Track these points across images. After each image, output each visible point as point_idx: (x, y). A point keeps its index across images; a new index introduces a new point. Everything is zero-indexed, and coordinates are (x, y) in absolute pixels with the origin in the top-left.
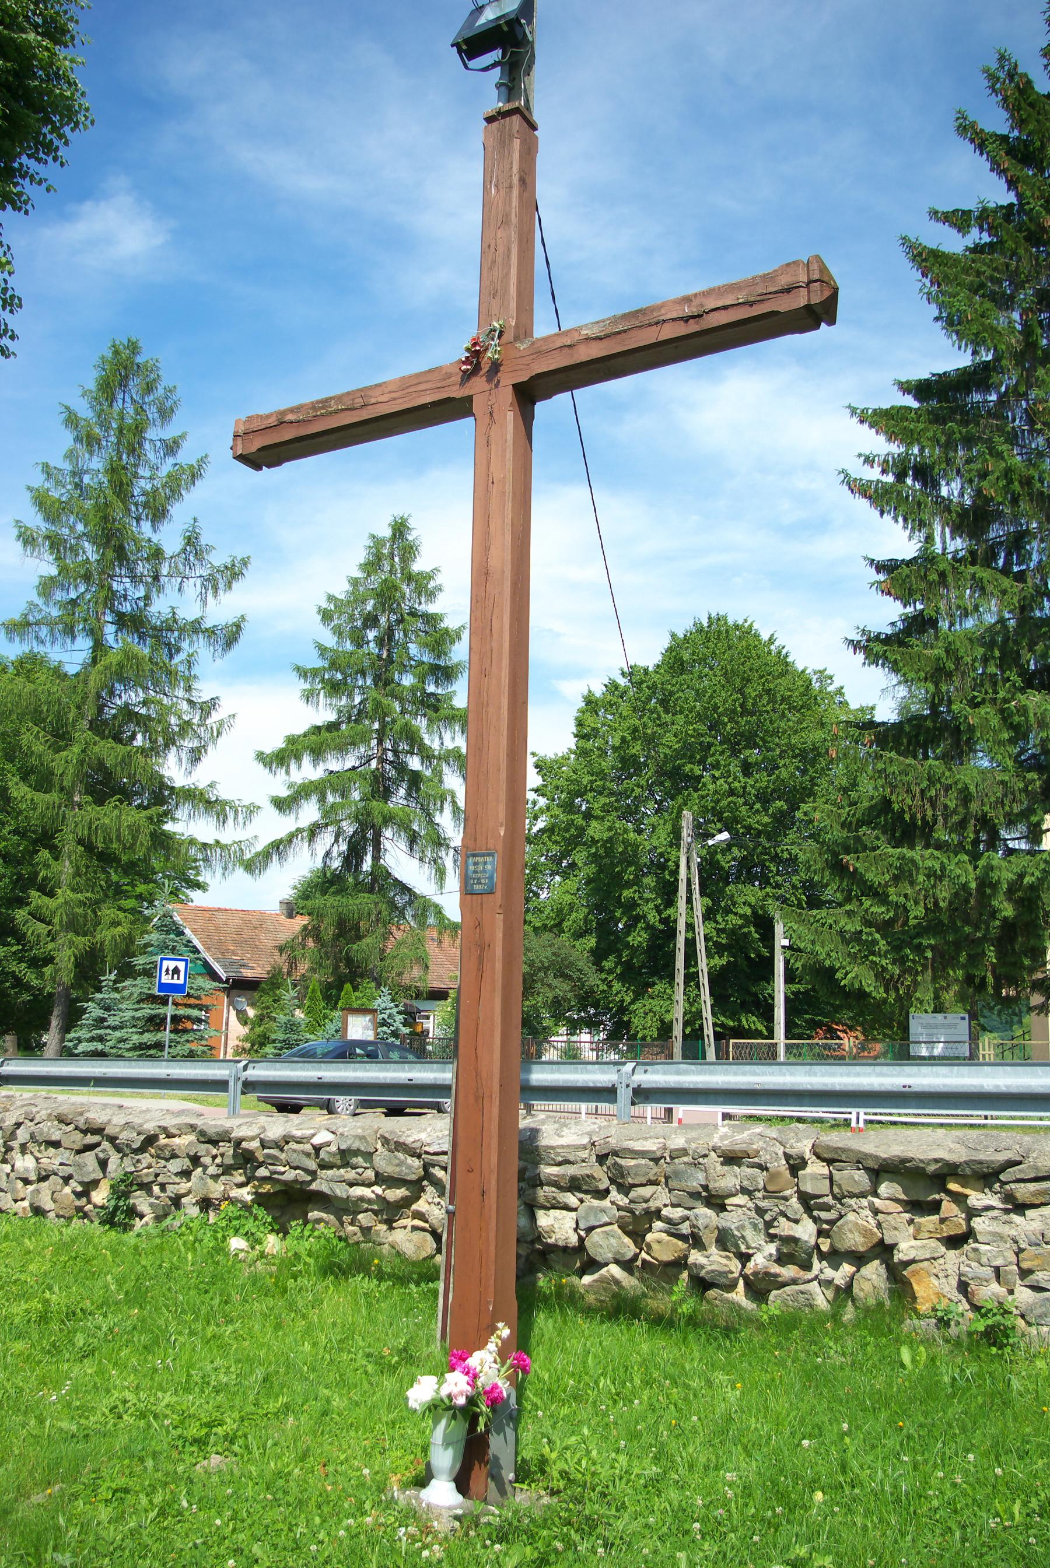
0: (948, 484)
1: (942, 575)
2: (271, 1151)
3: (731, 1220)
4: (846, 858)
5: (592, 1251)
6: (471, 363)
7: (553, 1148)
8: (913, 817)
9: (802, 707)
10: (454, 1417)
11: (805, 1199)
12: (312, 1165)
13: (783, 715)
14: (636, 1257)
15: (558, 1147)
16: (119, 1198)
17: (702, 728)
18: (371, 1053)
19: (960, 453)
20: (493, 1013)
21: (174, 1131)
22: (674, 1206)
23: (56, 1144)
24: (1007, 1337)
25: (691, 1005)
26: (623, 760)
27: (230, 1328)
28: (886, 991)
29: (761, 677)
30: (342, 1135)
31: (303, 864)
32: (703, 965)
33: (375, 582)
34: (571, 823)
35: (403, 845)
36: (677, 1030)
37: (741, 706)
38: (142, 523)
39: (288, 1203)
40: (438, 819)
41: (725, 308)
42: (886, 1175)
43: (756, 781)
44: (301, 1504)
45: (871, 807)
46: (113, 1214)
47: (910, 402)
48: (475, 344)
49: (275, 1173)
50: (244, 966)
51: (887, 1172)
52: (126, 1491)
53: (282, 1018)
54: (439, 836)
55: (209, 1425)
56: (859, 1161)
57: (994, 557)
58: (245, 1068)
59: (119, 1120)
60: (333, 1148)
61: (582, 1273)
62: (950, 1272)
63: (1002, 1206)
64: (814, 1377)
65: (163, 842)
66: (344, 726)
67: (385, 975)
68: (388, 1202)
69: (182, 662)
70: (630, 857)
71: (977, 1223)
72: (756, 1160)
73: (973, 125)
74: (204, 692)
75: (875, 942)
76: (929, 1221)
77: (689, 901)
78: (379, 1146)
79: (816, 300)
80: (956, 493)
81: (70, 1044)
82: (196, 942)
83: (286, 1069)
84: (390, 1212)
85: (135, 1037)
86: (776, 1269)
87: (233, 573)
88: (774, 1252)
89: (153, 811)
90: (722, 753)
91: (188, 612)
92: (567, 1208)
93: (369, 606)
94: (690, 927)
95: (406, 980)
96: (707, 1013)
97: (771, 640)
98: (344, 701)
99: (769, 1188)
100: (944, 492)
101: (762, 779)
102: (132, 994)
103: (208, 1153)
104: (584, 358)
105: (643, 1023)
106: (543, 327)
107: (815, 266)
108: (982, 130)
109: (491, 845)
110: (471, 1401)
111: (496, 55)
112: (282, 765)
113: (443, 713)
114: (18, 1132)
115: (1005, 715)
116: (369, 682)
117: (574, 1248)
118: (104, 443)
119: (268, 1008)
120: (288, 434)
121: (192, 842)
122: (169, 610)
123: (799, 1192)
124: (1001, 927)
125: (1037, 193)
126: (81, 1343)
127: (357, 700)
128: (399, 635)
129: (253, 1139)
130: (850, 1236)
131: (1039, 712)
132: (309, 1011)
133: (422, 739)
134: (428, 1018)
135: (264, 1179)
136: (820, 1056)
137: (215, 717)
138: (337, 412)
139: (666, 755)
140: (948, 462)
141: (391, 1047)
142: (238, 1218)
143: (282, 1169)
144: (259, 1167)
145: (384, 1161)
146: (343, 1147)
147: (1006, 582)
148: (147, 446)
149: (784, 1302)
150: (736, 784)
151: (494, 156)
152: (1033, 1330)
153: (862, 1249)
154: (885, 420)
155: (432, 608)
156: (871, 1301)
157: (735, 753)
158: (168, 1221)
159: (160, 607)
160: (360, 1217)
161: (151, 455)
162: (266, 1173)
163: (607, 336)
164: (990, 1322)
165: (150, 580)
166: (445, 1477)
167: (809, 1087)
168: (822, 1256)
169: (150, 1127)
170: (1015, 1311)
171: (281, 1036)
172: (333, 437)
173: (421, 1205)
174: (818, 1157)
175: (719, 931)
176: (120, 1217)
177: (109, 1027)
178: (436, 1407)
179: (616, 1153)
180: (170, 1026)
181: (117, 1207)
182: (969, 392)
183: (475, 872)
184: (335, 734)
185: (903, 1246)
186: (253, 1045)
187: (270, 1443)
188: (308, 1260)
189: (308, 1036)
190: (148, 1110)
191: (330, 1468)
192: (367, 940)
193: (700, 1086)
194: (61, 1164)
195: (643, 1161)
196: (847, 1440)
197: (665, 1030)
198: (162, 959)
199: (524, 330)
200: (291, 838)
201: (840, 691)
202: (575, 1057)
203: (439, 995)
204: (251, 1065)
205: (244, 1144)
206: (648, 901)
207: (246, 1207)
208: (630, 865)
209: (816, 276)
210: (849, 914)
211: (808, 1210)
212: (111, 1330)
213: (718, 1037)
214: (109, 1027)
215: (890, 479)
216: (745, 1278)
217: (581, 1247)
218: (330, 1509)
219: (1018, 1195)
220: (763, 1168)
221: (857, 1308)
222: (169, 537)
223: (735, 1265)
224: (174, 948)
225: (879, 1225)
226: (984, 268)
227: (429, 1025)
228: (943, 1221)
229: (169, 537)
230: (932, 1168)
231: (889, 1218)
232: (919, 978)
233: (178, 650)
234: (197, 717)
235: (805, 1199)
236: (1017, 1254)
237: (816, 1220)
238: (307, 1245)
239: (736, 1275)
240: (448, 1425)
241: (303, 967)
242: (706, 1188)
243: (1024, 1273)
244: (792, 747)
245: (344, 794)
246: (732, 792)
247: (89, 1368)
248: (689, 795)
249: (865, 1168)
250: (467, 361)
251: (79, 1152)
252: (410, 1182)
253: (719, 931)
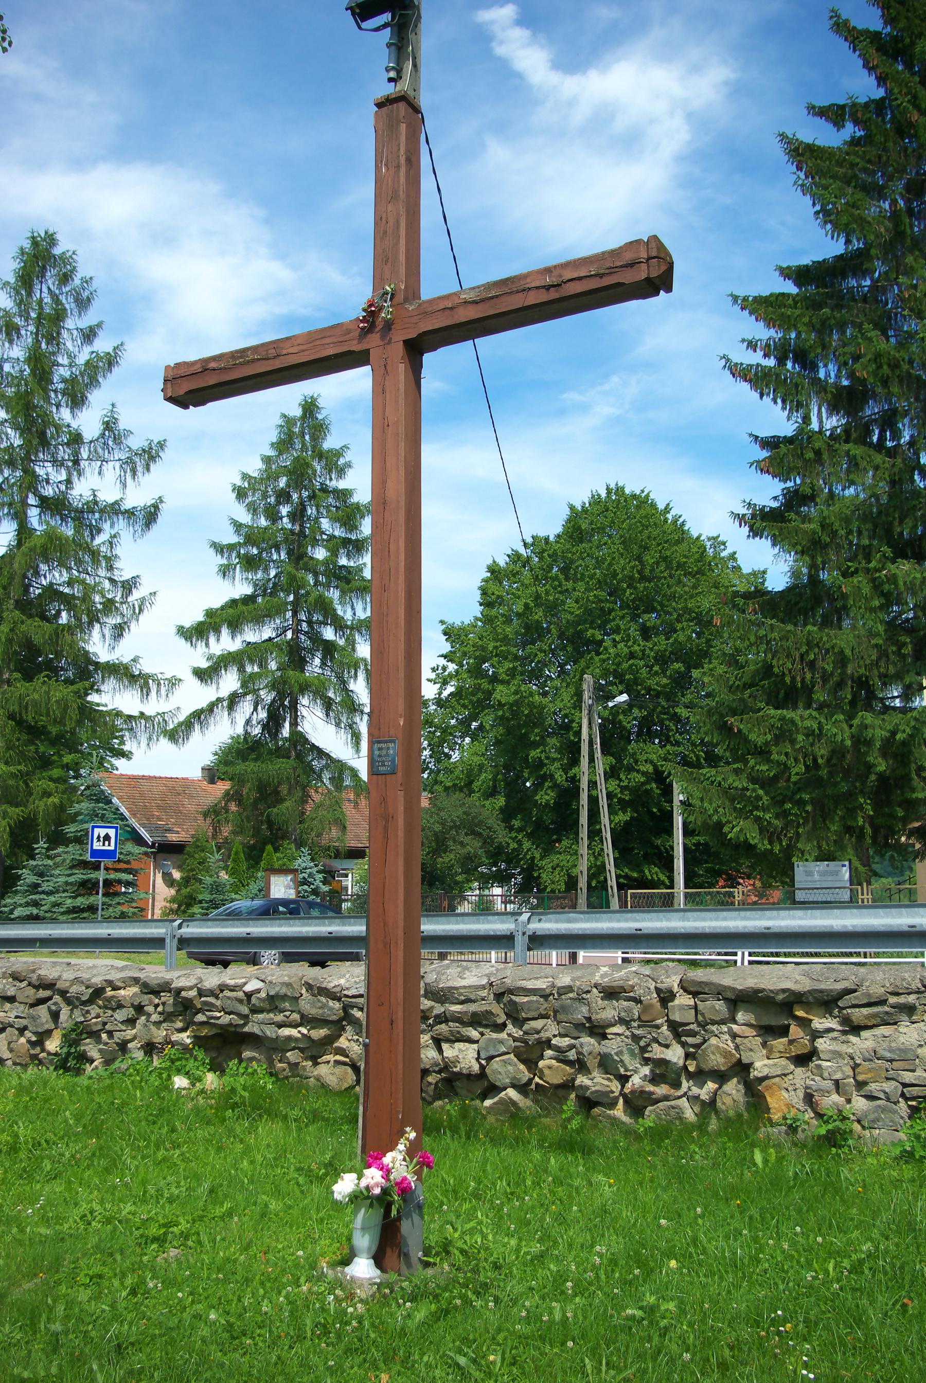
0: (826, 366)
1: (818, 453)
2: (208, 999)
3: (611, 1046)
4: (731, 720)
5: (491, 1078)
6: (367, 322)
7: (456, 988)
8: (793, 679)
9: (697, 573)
10: (371, 1205)
11: (674, 1026)
12: (245, 1010)
13: (679, 582)
14: (530, 1081)
15: (461, 987)
16: (70, 1046)
17: (603, 594)
18: (292, 909)
19: (835, 337)
20: (400, 874)
21: (119, 984)
22: (561, 1035)
23: (11, 999)
24: (846, 1140)
25: (596, 858)
26: (527, 627)
27: (178, 1152)
28: (771, 843)
29: (659, 545)
30: (271, 982)
31: (224, 730)
32: (605, 819)
33: (287, 461)
34: (478, 688)
35: (319, 711)
36: (583, 883)
37: (638, 572)
38: (62, 410)
39: (224, 1044)
40: (352, 686)
41: (580, 279)
42: (743, 1005)
43: (655, 644)
44: (247, 1281)
45: (757, 670)
46: (66, 1060)
47: (790, 288)
48: (370, 306)
49: (212, 1018)
50: (169, 830)
51: (743, 1001)
52: (100, 1276)
53: (208, 880)
54: (353, 702)
55: (167, 1225)
56: (720, 992)
57: (869, 433)
58: (180, 926)
59: (69, 975)
60: (263, 995)
61: (484, 1096)
62: (798, 1086)
63: (840, 1028)
64: (682, 1176)
65: (89, 713)
66: (260, 599)
67: (305, 836)
68: (313, 1041)
69: (103, 543)
70: (536, 718)
71: (822, 1044)
72: (632, 994)
73: (846, 22)
74: (124, 571)
75: (759, 798)
76: (780, 1043)
77: (592, 759)
78: (304, 991)
79: (654, 274)
80: (833, 375)
81: (6, 909)
82: (123, 809)
83: (217, 926)
84: (315, 1051)
85: (69, 901)
86: (650, 1088)
87: (150, 455)
88: (647, 1073)
89: (79, 686)
90: (622, 618)
91: (108, 495)
92: (470, 1041)
93: (282, 482)
94: (593, 784)
95: (324, 842)
96: (611, 866)
97: (667, 509)
98: (260, 575)
99: (643, 1018)
100: (822, 374)
101: (661, 643)
102: (64, 860)
103: (151, 1003)
104: (463, 319)
105: (551, 878)
106: (429, 290)
107: (653, 245)
108: (854, 28)
109: (392, 733)
110: (385, 1191)
111: (386, 17)
112: (202, 638)
113: (355, 584)
115: (877, 585)
116: (283, 556)
117: (476, 1075)
118: (23, 332)
119: (193, 870)
120: (212, 380)
121: (118, 714)
122: (90, 492)
123: (668, 1021)
124: (877, 780)
125: (904, 90)
126: (49, 1167)
127: (273, 573)
128: (311, 511)
129: (191, 988)
130: (713, 1057)
131: (908, 580)
132: (233, 873)
133: (335, 610)
134: (346, 876)
135: (202, 1023)
136: (722, 903)
137: (136, 595)
138: (253, 361)
139: (568, 621)
140: (824, 347)
141: (312, 905)
142: (179, 1059)
143: (218, 1015)
144: (197, 1014)
145: (307, 1004)
146: (272, 993)
147: (879, 458)
148: (65, 334)
149: (658, 1116)
150: (636, 648)
151: (385, 135)
152: (867, 1133)
153: (723, 1069)
154: (764, 307)
155: (342, 485)
156: (731, 1113)
157: (635, 617)
158: (117, 1064)
159: (81, 491)
160: (288, 1054)
161: (69, 344)
162: (204, 1019)
163: (482, 301)
164: (830, 1127)
165: (70, 464)
166: (365, 1255)
167: (683, 931)
168: (690, 1076)
169: (97, 980)
170: (852, 1117)
171: (208, 897)
172: (251, 382)
173: (343, 1042)
174: (685, 990)
175: (623, 789)
176: (71, 1063)
177: (43, 892)
178: (356, 1197)
179: (511, 991)
180: (101, 890)
181: (69, 1054)
182: (844, 277)
183: (380, 756)
184: (251, 606)
185: (758, 1064)
186: (179, 907)
187: (218, 1238)
188: (243, 1093)
189: (233, 896)
190: (94, 966)
191: (270, 1256)
192: (287, 804)
193: (588, 932)
194: (17, 1017)
195: (535, 998)
196: (700, 1221)
197: (572, 883)
198: (93, 827)
199: (413, 292)
200: (211, 708)
201: (733, 557)
202: (488, 909)
203: (356, 854)
204: (185, 924)
205: (183, 994)
206: (554, 760)
207: (185, 1049)
208: (535, 725)
209: (654, 254)
210: (737, 772)
211: (677, 1036)
212: (73, 1156)
213: (620, 887)
214: (43, 892)
215: (771, 362)
216: (624, 1096)
217: (482, 1074)
218: (273, 1284)
219: (854, 1018)
220: (638, 1001)
221: (719, 1119)
222: (88, 422)
223: (615, 1086)
224: (103, 815)
225: (737, 1048)
226: (858, 160)
227: (348, 882)
228: (791, 1042)
229: (88, 422)
230: (780, 997)
231: (746, 1041)
232: (800, 830)
233: (99, 531)
234: (119, 595)
235: (674, 1026)
236: (854, 1069)
237: (684, 1045)
238: (242, 1080)
239: (616, 1094)
240: (366, 1212)
241: (226, 830)
242: (589, 1019)
243: (860, 1085)
244: (686, 610)
245: (263, 664)
246: (632, 656)
247: (58, 1187)
248: (591, 658)
249: (724, 999)
250: (364, 320)
251: (32, 1006)
252: (332, 1022)
253: (623, 789)
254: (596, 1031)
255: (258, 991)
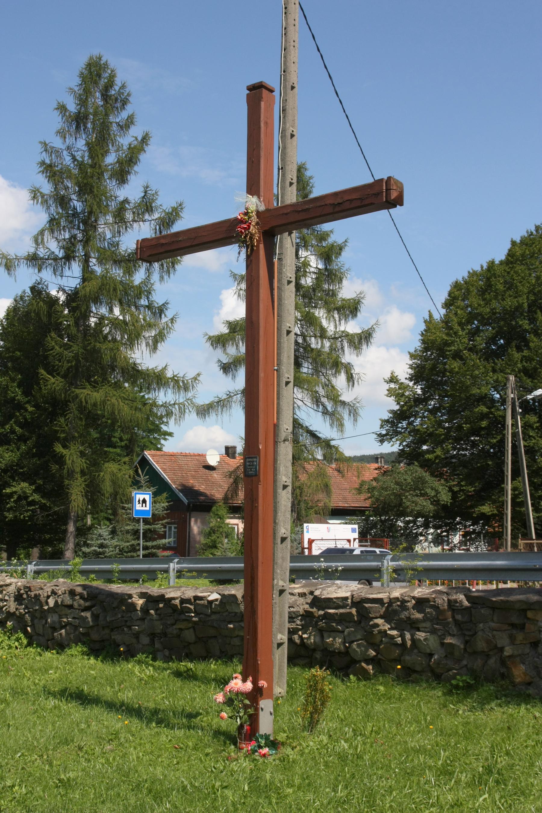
5: (352, 655)
114: (49, 600)
222: (131, 192)
254: (414, 625)
255: (216, 600)
